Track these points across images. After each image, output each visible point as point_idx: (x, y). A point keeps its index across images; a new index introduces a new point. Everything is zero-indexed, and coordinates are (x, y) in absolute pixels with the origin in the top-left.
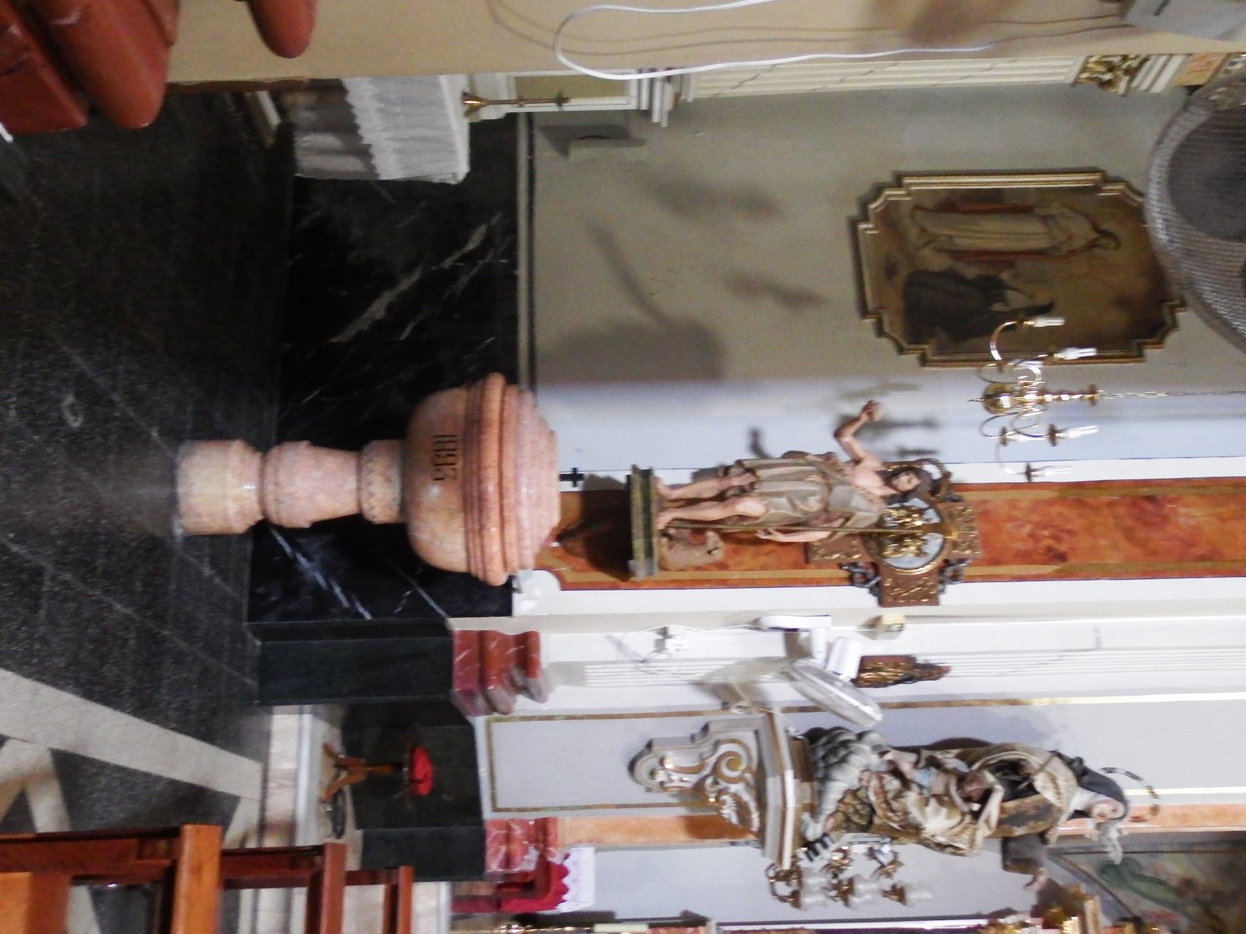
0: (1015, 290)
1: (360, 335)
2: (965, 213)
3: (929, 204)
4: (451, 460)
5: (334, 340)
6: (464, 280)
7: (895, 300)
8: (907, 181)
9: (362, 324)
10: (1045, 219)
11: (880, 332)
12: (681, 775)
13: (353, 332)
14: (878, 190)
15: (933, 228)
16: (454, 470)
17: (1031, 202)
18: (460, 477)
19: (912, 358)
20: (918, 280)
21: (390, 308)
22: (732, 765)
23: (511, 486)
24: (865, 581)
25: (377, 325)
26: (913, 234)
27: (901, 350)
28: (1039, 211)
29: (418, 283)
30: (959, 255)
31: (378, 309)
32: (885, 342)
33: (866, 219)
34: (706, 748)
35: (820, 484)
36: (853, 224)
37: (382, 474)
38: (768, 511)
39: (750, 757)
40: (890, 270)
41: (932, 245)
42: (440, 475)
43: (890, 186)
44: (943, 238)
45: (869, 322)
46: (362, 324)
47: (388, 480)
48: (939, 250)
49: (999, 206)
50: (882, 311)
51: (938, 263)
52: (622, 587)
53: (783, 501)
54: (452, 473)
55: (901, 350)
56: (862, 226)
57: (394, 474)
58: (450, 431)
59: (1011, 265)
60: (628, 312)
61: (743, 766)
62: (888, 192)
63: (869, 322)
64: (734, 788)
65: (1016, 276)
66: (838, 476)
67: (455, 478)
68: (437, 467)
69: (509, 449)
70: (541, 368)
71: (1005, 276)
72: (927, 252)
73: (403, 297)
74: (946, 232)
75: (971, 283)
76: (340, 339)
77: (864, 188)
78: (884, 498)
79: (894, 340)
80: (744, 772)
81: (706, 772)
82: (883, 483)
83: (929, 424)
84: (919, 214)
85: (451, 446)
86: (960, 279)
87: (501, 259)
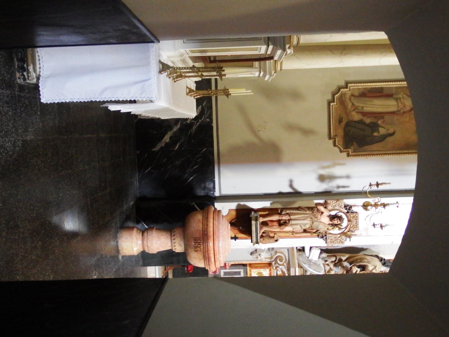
0: (383, 127)
1: (162, 148)
2: (369, 97)
3: (356, 93)
4: (199, 246)
5: (153, 150)
6: (195, 127)
7: (341, 132)
8: (349, 85)
9: (162, 144)
10: (397, 99)
11: (335, 145)
12: (265, 259)
13: (159, 147)
14: (339, 88)
15: (356, 104)
16: (200, 249)
17: (394, 91)
18: (202, 251)
19: (345, 154)
20: (350, 124)
21: (171, 138)
22: (281, 261)
23: (218, 253)
24: (322, 237)
25: (166, 144)
26: (350, 105)
27: (341, 151)
28: (394, 96)
29: (180, 128)
30: (365, 114)
31: (167, 138)
32: (336, 148)
33: (333, 101)
34: (273, 252)
35: (310, 221)
36: (329, 103)
37: (178, 243)
38: (293, 230)
39: (286, 259)
40: (340, 121)
41: (356, 110)
42: (197, 250)
43: (344, 88)
44: (360, 107)
45: (331, 141)
46: (162, 144)
47: (180, 245)
48: (358, 112)
49: (381, 94)
50: (336, 137)
51: (356, 117)
52: (249, 239)
53: (299, 226)
54: (200, 250)
55: (341, 151)
56: (332, 104)
57: (182, 243)
58: (198, 236)
59: (383, 118)
60: (250, 138)
61: (284, 261)
62: (342, 90)
63: (331, 141)
64: (281, 267)
65: (383, 122)
66: (316, 219)
67: (201, 251)
68: (195, 248)
69: (216, 242)
70: (222, 159)
71: (380, 122)
72: (354, 113)
73: (175, 133)
74: (362, 105)
75: (368, 125)
76: (156, 149)
77: (334, 88)
78: (329, 224)
79: (339, 148)
80: (284, 263)
81: (273, 259)
82: (329, 220)
83: (348, 177)
84: (352, 98)
85: (199, 241)
86: (365, 124)
87: (207, 119)
